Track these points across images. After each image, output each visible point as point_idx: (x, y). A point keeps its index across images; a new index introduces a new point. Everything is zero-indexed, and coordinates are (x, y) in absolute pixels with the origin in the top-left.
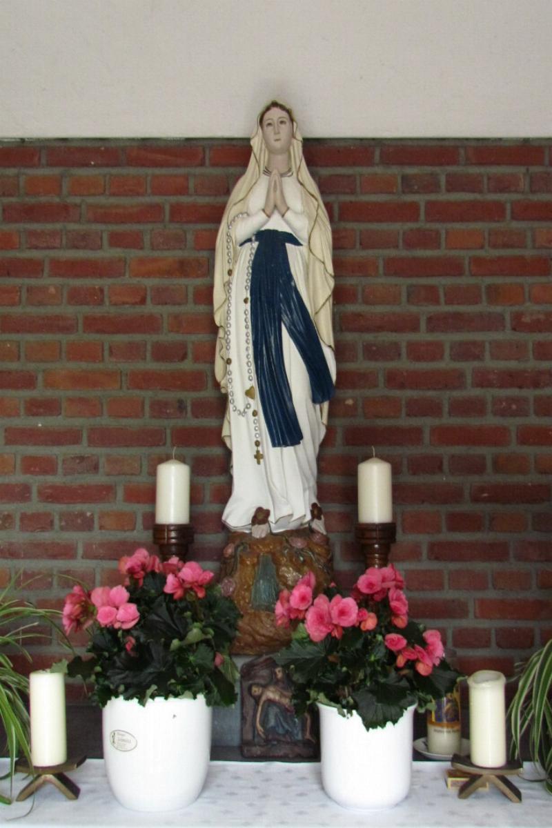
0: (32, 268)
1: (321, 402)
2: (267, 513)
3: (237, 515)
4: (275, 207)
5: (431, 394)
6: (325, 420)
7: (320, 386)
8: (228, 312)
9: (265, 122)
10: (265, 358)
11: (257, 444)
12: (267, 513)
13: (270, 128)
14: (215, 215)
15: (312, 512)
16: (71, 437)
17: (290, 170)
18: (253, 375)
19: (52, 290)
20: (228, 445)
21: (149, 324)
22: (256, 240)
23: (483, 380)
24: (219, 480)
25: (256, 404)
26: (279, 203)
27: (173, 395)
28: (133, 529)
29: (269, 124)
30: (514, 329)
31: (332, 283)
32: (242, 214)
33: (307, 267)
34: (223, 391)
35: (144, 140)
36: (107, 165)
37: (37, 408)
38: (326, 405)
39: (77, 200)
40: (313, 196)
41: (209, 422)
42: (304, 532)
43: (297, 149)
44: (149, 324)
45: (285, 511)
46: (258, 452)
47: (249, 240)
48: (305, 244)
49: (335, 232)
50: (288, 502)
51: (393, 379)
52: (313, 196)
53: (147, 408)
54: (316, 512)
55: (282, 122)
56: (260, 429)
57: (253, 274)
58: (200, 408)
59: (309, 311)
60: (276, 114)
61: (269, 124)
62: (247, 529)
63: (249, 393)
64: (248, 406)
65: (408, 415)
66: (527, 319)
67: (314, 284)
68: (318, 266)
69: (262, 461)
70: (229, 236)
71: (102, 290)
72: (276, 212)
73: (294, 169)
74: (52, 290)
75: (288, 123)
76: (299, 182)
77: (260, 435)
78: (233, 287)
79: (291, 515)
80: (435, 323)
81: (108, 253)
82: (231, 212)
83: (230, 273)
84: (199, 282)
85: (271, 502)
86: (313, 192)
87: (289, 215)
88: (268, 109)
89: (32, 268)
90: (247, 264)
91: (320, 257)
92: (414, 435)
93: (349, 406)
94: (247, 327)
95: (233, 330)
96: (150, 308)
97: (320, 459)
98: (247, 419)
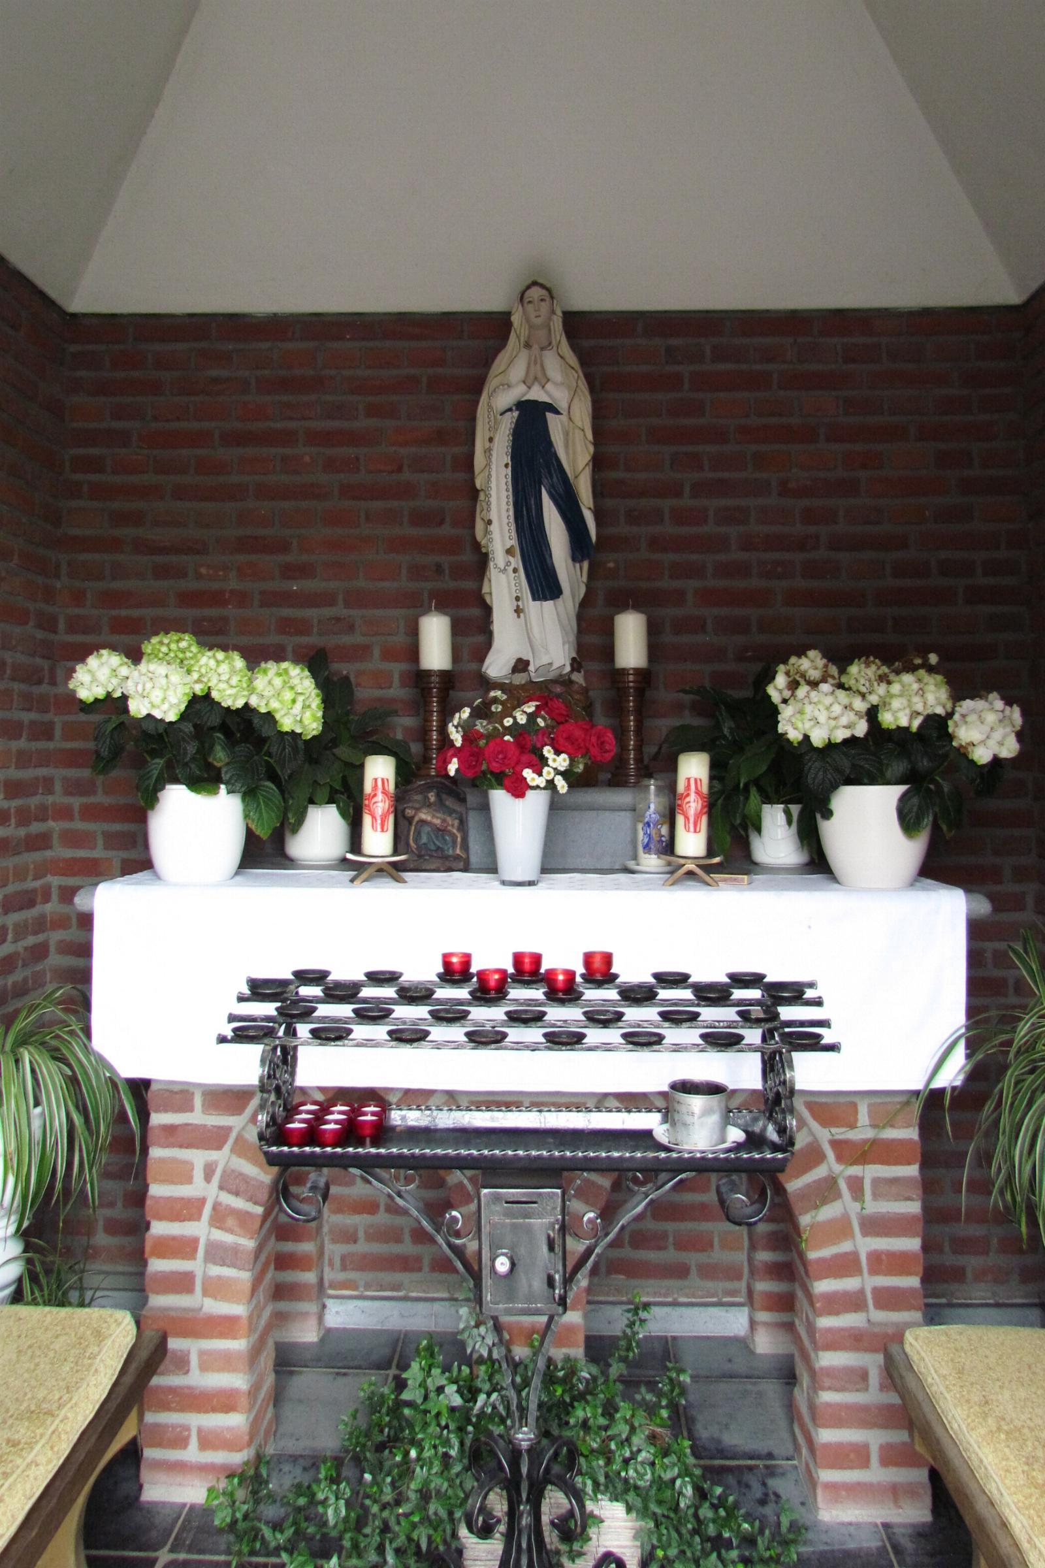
0: (287, 438)
1: (581, 561)
2: (527, 663)
3: (497, 666)
4: (536, 378)
5: (694, 557)
6: (585, 579)
7: (579, 545)
8: (489, 476)
9: (526, 300)
10: (525, 518)
11: (517, 599)
12: (527, 663)
13: (530, 306)
14: (476, 387)
15: (572, 665)
16: (327, 599)
17: (550, 344)
18: (514, 534)
19: (307, 459)
20: (488, 601)
21: (407, 491)
22: (517, 409)
23: (747, 544)
24: (480, 639)
25: (517, 562)
26: (539, 375)
27: (431, 559)
28: (390, 687)
29: (530, 302)
30: (780, 495)
31: (591, 449)
32: (503, 385)
33: (566, 434)
34: (484, 550)
35: (400, 314)
36: (363, 339)
37: (291, 572)
38: (586, 565)
39: (333, 372)
40: (573, 368)
41: (469, 585)
42: (565, 681)
43: (557, 323)
44: (407, 491)
45: (545, 660)
46: (518, 606)
47: (510, 410)
48: (565, 413)
49: (595, 403)
50: (547, 651)
51: (655, 543)
52: (573, 368)
53: (404, 571)
54: (575, 665)
55: (542, 300)
56: (520, 585)
57: (514, 441)
58: (459, 572)
59: (569, 475)
60: (535, 292)
61: (530, 302)
62: (506, 678)
63: (509, 552)
64: (508, 564)
65: (671, 577)
66: (792, 485)
67: (574, 453)
68: (578, 435)
69: (522, 615)
70: (490, 407)
71: (357, 459)
72: (536, 384)
73: (554, 343)
74: (307, 459)
75: (548, 299)
76: (559, 354)
77: (521, 590)
78: (494, 453)
79: (551, 664)
80: (699, 489)
81: (362, 423)
82: (492, 383)
83: (491, 440)
84: (458, 450)
85: (531, 654)
86: (573, 365)
87: (549, 386)
88: (528, 287)
89: (287, 438)
90: (508, 432)
91: (580, 424)
92: (679, 597)
93: (610, 569)
94: (507, 490)
95: (493, 493)
96: (407, 476)
97: (580, 617)
98: (508, 576)
